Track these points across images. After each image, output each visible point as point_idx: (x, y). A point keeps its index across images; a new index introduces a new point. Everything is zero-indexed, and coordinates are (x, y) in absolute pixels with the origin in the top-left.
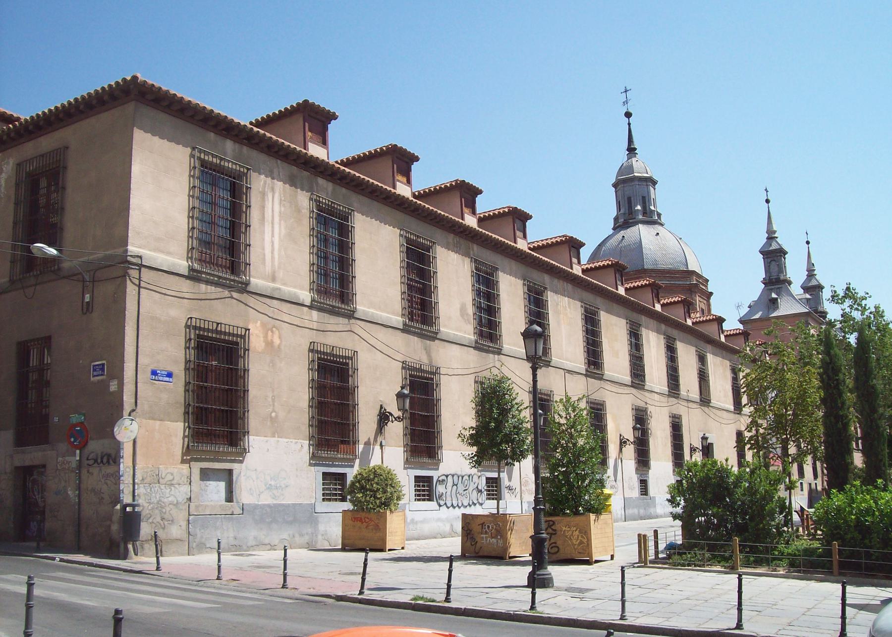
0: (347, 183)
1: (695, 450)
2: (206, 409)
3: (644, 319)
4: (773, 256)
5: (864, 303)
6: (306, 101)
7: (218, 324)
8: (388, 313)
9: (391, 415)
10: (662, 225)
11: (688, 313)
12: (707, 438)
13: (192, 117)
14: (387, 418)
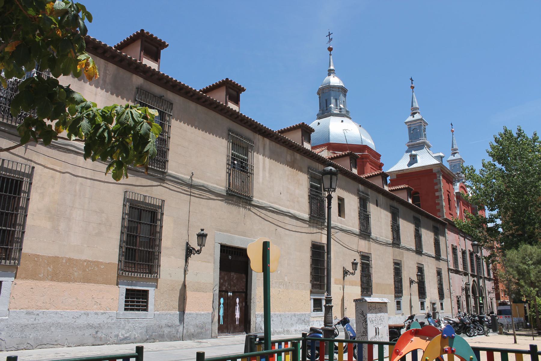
0: (225, 113)
1: (412, 282)
6: (303, 123)
7: (3, 160)
8: (212, 183)
9: (194, 249)
13: (192, 96)
14: (346, 273)
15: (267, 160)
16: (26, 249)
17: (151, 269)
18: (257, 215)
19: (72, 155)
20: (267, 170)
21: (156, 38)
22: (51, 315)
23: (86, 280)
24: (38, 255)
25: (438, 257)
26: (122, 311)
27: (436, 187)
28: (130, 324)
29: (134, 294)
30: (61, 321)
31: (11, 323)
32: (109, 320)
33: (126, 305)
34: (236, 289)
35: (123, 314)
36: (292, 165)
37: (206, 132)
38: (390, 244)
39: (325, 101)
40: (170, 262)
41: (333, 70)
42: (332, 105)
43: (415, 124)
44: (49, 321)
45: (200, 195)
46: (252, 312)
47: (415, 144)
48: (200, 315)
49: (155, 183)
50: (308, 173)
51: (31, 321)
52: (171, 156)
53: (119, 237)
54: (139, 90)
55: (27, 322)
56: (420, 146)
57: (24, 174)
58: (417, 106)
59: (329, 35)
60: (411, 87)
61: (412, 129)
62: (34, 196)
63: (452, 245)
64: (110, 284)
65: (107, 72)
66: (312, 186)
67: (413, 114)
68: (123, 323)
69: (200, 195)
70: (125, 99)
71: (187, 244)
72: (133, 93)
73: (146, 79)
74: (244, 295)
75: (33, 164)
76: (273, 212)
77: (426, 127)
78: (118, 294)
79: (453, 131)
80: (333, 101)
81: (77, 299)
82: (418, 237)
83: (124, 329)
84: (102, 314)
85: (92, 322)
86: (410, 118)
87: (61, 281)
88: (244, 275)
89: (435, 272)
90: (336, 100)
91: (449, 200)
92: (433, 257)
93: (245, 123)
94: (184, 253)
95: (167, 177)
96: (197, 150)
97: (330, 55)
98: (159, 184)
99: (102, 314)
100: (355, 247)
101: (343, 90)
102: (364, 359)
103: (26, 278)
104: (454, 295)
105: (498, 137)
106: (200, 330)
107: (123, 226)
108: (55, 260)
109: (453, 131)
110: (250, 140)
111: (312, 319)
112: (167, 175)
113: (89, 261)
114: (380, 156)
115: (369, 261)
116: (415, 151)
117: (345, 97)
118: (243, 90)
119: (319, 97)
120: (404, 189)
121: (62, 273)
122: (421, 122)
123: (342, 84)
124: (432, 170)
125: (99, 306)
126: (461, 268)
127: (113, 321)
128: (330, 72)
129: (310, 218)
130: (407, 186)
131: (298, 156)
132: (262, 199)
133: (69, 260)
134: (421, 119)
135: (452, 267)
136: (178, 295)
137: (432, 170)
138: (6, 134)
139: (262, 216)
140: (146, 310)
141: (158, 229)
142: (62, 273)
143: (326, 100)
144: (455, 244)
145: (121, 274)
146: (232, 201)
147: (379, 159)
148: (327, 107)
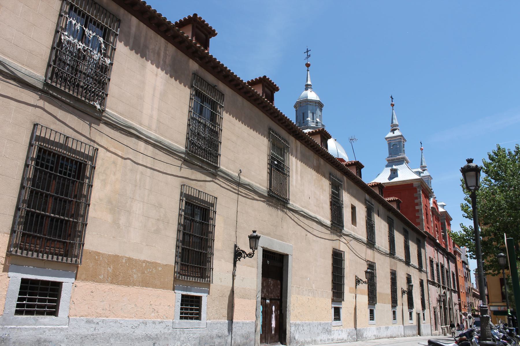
1: (359, 282)
2: (62, 221)
5: (514, 153)
7: (67, 137)
8: (256, 182)
9: (244, 252)
12: (257, 238)
13: (240, 89)
15: (299, 163)
16: (87, 246)
17: (202, 273)
18: (291, 218)
19: (134, 140)
20: (299, 174)
21: (207, 25)
22: (111, 324)
23: (145, 283)
24: (99, 253)
25: (420, 269)
26: (178, 320)
27: (416, 201)
28: (185, 335)
29: (192, 301)
30: (120, 331)
31: (71, 333)
32: (166, 331)
33: (181, 313)
34: (272, 296)
35: (179, 323)
36: (318, 169)
37: (251, 128)
38: (388, 254)
39: (302, 114)
40: (221, 264)
42: (309, 119)
43: (395, 140)
44: (109, 331)
45: (246, 194)
46: (287, 320)
47: (394, 159)
48: (246, 324)
49: (209, 179)
50: (330, 179)
51: (91, 331)
52: (223, 150)
53: (175, 236)
54: (195, 75)
55: (86, 333)
56: (401, 161)
57: (87, 156)
58: (397, 123)
59: (307, 52)
60: (392, 104)
61: (392, 145)
62: (96, 183)
63: (430, 257)
64: (167, 289)
65: (167, 52)
66: (333, 193)
67: (393, 131)
68: (178, 333)
69: (246, 194)
70: (182, 84)
71: (236, 246)
72: (190, 78)
73: (201, 65)
74: (278, 302)
75: (96, 146)
76: (304, 216)
77: (405, 143)
78: (173, 299)
79: (422, 149)
80: (310, 115)
81: (136, 305)
82: (407, 248)
83: (179, 340)
84: (160, 323)
85: (150, 333)
86: (390, 134)
87: (121, 284)
88: (279, 281)
89: (389, 271)
90: (313, 114)
91: (427, 214)
92: (417, 269)
93: (282, 123)
94: (232, 256)
95: (219, 173)
96: (243, 148)
97: (308, 70)
98: (211, 179)
99: (160, 323)
100: (363, 256)
101: (319, 105)
103: (85, 280)
104: (432, 306)
105: (492, 154)
106: (245, 341)
107: (179, 224)
108: (115, 259)
109: (422, 149)
110: (285, 140)
111: (333, 328)
112: (219, 171)
113: (148, 262)
115: (373, 270)
116: (395, 165)
117: (321, 112)
118: (277, 89)
119: (296, 111)
120: (394, 201)
121: (121, 274)
122: (401, 139)
123: (318, 99)
124: (412, 184)
125: (157, 314)
126: (436, 281)
127: (170, 331)
128: (307, 87)
129: (332, 224)
130: (397, 198)
131: (322, 161)
132: (295, 203)
133: (129, 259)
134: (401, 136)
135: (430, 279)
136: (227, 302)
137: (412, 184)
138: (71, 108)
139: (296, 220)
140: (199, 318)
141: (210, 229)
142: (121, 274)
143: (303, 114)
144: (432, 257)
145: (177, 278)
146: (272, 202)
148: (304, 120)
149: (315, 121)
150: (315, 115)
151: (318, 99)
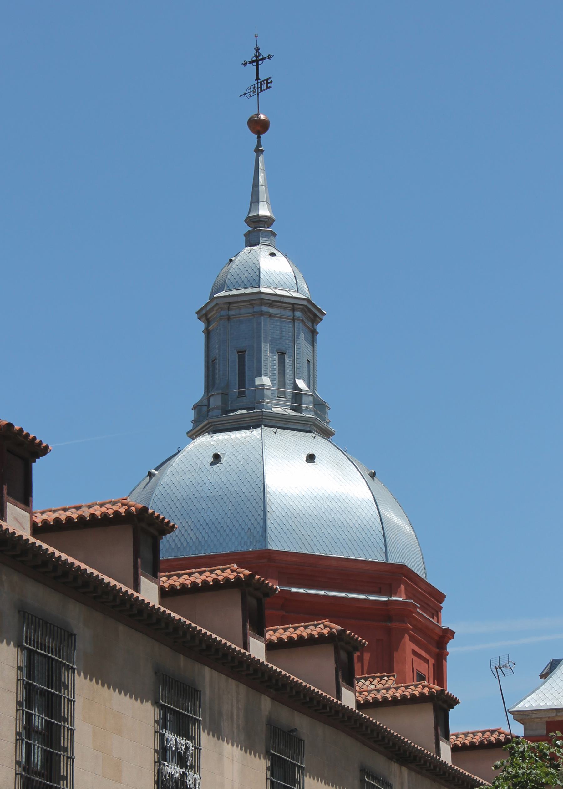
3: (208, 678)
4: (257, 49)
10: (327, 434)
11: (347, 677)
39: (234, 357)
41: (268, 221)
42: (266, 381)
59: (257, 60)
80: (269, 358)
97: (259, 151)
101: (308, 315)
102: (560, 719)
114: (440, 597)
117: (313, 342)
118: (39, 450)
119: (208, 333)
120: (321, 640)
128: (257, 230)
147: (436, 611)
148: (242, 384)
149: (289, 391)
150: (288, 361)
151: (303, 292)
